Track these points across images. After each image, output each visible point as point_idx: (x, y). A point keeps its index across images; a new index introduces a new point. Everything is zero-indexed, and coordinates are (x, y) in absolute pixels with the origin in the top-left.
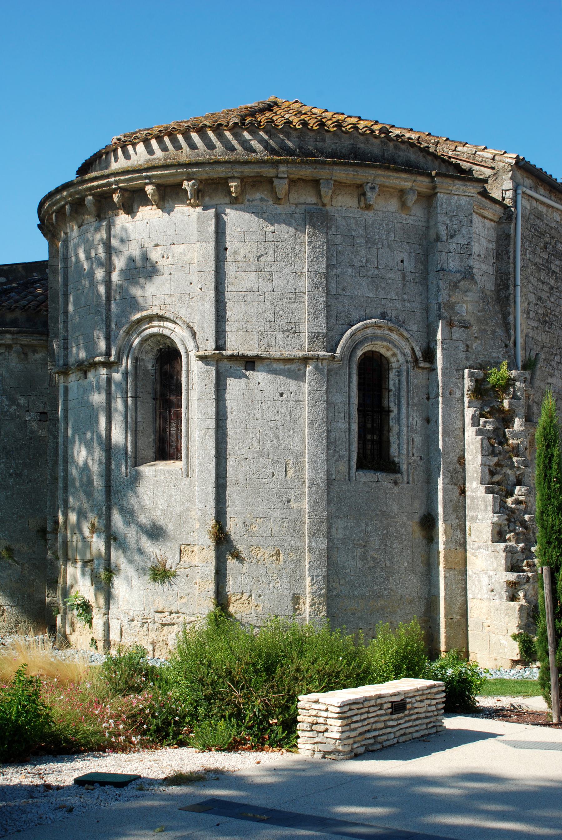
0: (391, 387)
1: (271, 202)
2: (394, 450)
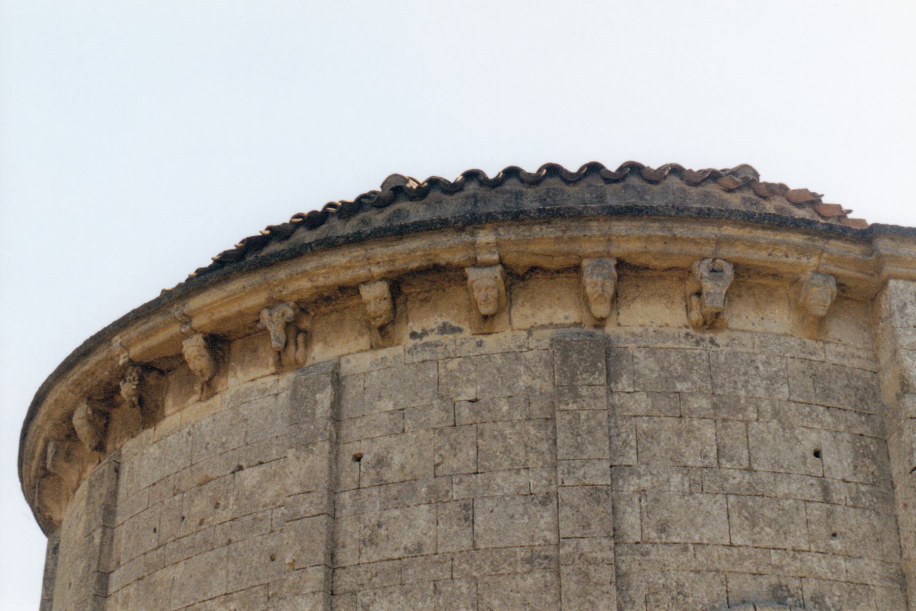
1: (467, 333)
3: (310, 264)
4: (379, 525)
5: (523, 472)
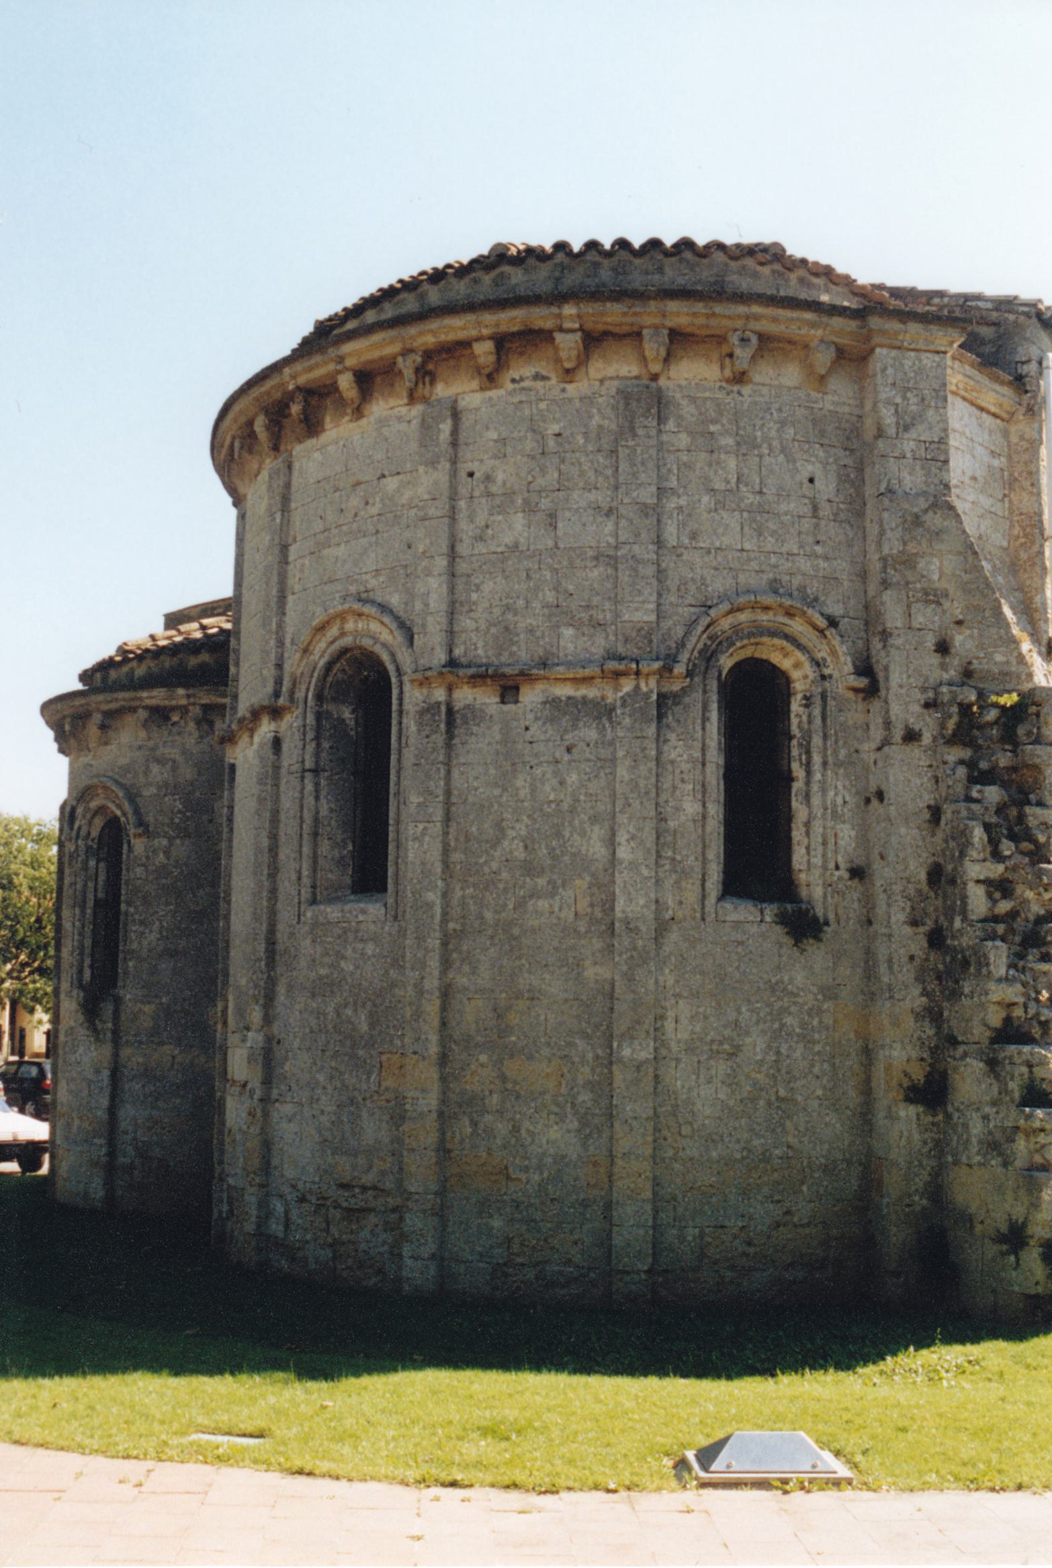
0: (794, 729)
1: (554, 381)
2: (799, 857)
3: (434, 324)
4: (487, 527)
5: (594, 491)
